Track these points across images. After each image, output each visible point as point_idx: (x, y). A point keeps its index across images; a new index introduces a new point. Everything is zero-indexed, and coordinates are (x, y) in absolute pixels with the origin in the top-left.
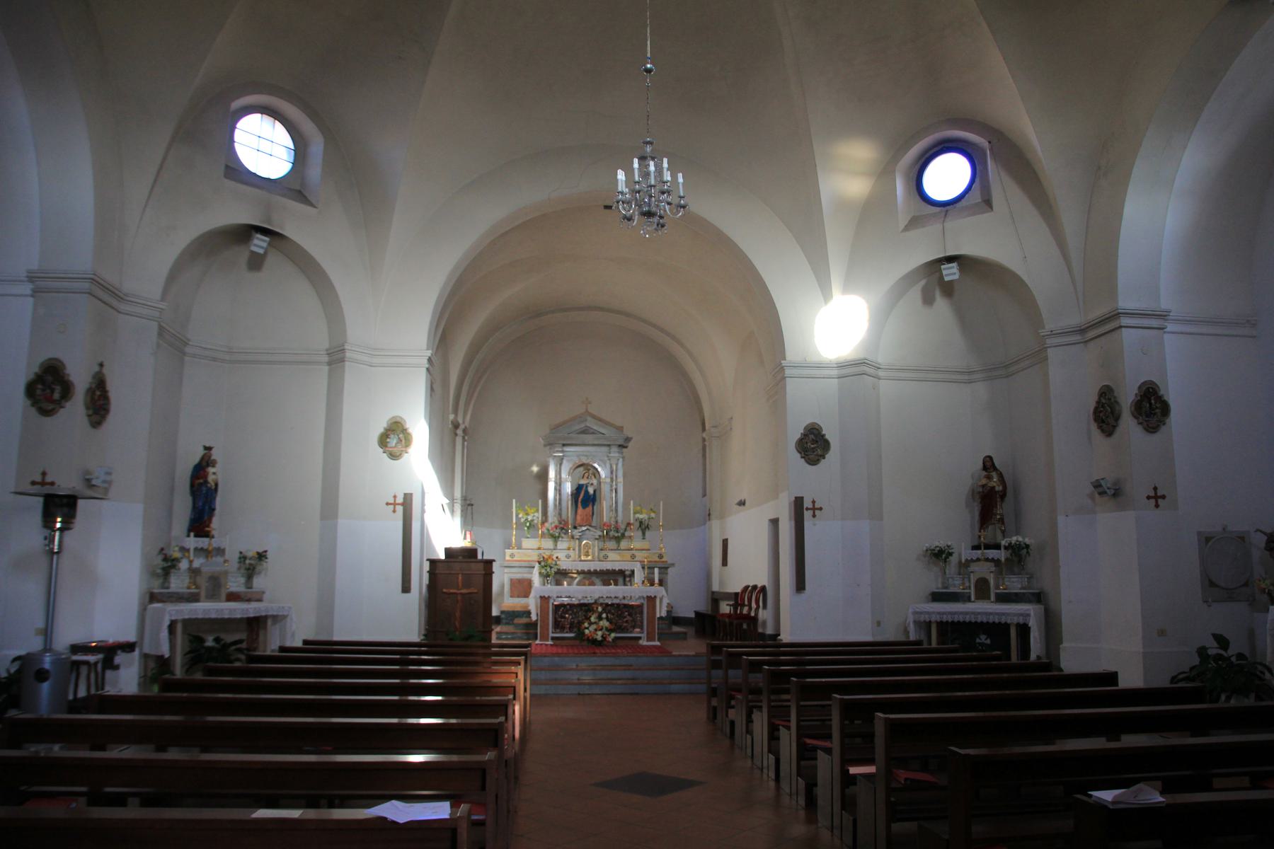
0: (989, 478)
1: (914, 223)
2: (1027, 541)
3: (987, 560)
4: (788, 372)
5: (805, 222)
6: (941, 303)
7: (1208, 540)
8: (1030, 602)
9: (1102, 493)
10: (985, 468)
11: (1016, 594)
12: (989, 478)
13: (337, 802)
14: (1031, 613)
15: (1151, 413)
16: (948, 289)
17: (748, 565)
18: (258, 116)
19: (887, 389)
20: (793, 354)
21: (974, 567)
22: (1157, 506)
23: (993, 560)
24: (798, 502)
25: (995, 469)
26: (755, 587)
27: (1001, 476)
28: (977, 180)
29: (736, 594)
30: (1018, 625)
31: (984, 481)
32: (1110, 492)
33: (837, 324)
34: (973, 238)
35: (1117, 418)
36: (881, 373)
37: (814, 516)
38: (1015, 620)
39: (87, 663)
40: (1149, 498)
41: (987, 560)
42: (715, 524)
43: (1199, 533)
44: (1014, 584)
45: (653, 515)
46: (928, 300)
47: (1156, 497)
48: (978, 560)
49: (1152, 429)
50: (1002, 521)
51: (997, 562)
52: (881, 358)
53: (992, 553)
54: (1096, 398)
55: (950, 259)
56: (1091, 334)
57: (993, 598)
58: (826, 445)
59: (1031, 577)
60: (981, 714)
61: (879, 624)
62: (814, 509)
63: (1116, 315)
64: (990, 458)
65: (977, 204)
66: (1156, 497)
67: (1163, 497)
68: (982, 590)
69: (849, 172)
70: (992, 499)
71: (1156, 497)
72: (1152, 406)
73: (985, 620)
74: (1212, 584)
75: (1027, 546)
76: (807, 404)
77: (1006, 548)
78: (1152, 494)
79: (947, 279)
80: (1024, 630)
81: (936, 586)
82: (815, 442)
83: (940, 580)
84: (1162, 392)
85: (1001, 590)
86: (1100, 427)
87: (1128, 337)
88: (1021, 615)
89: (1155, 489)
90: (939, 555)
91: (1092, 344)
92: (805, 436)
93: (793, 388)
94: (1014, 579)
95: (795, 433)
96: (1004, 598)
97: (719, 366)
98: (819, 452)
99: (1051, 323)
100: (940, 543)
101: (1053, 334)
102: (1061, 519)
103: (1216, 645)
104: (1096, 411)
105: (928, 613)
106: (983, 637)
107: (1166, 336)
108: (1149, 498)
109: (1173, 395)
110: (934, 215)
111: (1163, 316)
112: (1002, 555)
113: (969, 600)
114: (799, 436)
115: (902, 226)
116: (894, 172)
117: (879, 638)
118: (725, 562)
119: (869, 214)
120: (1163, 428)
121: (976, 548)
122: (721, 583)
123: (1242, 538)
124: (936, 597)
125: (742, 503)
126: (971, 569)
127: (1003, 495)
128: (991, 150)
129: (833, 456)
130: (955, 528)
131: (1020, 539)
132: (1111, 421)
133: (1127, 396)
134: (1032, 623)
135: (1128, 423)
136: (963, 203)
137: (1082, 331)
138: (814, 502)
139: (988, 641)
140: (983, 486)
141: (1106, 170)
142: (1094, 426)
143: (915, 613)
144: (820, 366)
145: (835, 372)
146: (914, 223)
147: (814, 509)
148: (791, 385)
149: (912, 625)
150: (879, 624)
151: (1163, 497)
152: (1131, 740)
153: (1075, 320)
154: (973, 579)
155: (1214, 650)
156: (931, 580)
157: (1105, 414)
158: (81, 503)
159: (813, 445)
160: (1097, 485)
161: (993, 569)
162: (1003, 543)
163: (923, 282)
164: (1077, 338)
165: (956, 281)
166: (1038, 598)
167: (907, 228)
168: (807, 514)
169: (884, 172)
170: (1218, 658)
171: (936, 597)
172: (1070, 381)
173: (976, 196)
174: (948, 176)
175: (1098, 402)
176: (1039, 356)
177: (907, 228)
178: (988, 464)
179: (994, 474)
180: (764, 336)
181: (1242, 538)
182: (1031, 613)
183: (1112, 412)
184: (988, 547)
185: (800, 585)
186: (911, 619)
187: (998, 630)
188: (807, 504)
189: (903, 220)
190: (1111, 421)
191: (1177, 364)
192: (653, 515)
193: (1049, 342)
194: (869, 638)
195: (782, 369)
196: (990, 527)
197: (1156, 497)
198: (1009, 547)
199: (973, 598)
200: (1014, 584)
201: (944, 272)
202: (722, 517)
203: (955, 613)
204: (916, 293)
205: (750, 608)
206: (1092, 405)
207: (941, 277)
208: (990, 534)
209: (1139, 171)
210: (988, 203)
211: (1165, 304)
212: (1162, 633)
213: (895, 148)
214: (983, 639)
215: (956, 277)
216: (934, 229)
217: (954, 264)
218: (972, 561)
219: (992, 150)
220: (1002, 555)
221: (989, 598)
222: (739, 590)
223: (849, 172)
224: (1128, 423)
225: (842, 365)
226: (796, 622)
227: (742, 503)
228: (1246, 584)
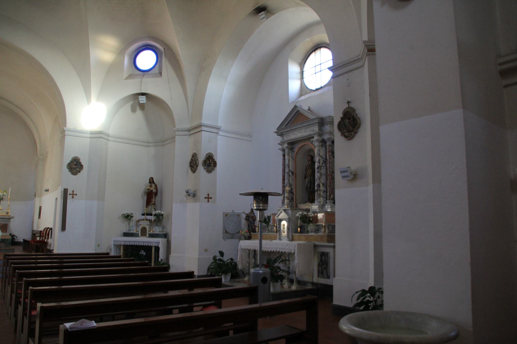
0: (151, 186)
1: (130, 76)
2: (162, 213)
3: (147, 220)
4: (66, 133)
5: (82, 67)
6: (139, 112)
7: (226, 215)
8: (162, 237)
9: (189, 195)
10: (150, 182)
11: (157, 234)
12: (151, 186)
13: (32, 327)
14: (161, 242)
15: (209, 165)
16: (142, 107)
17: (48, 219)
18: (313, 54)
19: (112, 145)
20: (70, 124)
21: (141, 223)
22: (208, 201)
23: (149, 220)
24: (65, 191)
25: (154, 183)
26: (48, 228)
27: (156, 186)
28: (158, 64)
29: (41, 231)
30: (155, 247)
31: (149, 188)
32: (192, 195)
33: (92, 113)
34: (153, 87)
35: (197, 166)
36: (110, 138)
37: (73, 197)
38: (154, 245)
39: (151, 262)
40: (205, 198)
41: (147, 220)
42: (37, 199)
43: (223, 213)
44: (157, 230)
45: (5, 193)
46: (133, 110)
47: (208, 198)
48: (143, 220)
49: (209, 171)
50: (154, 204)
51: (150, 221)
52: (110, 132)
53: (149, 217)
54: (191, 157)
55: (143, 94)
56: (192, 132)
57: (147, 235)
58: (81, 167)
59: (163, 228)
60: (141, 283)
61: (99, 245)
62: (73, 194)
63: (200, 126)
64: (152, 178)
65: (157, 73)
66: (208, 198)
67: (211, 198)
68: (144, 232)
69: (104, 49)
70: (152, 195)
71: (208, 198)
72: (210, 163)
73: (133, 244)
74: (226, 232)
75: (162, 215)
76: (74, 148)
77: (155, 215)
78: (207, 197)
79: (141, 102)
80: (157, 249)
81: (125, 230)
82: (76, 165)
83: (128, 228)
84: (214, 158)
85: (151, 232)
86: (191, 169)
87: (205, 135)
88: (157, 243)
89: (208, 195)
90: (128, 217)
91: (192, 136)
92: (72, 162)
93: (68, 140)
94: (157, 228)
95: (68, 160)
96: (152, 236)
97: (44, 127)
98: (78, 169)
99: (178, 126)
100: (129, 212)
101: (178, 130)
102: (174, 204)
103: (219, 255)
104: (191, 163)
105: (119, 241)
106: (143, 251)
107: (219, 137)
108: (205, 198)
109: (219, 159)
110: (139, 75)
111: (218, 129)
112: (152, 218)
113: (138, 236)
114: (69, 162)
115: (125, 77)
116: (124, 53)
117: (98, 251)
118: (39, 216)
119: (112, 69)
120: (213, 172)
121: (143, 215)
122: (38, 227)
123: (239, 215)
124: (126, 235)
125: (47, 190)
126: (140, 223)
127: (156, 194)
128: (164, 52)
129: (84, 172)
130: (136, 206)
131: (160, 212)
132: (195, 167)
133: (201, 158)
134: (160, 246)
135: (201, 169)
136: (151, 72)
137: (189, 130)
138: (73, 191)
139: (144, 254)
140: (148, 189)
141: (204, 69)
142: (189, 168)
143: (114, 241)
144: (82, 132)
145: (89, 136)
146: (130, 76)
147: (73, 194)
148: (67, 139)
149: (113, 246)
150: (99, 245)
151: (211, 198)
152: (172, 293)
153: (187, 126)
154: (140, 227)
155: (219, 257)
156: (124, 227)
157: (193, 165)
158: (270, 197)
159: (75, 166)
160: (187, 192)
161: (148, 224)
162: (153, 213)
163: (132, 102)
164: (187, 133)
165: (144, 102)
166: (166, 236)
167: (127, 78)
168: (69, 197)
169: (121, 53)
170: (220, 260)
171: (126, 235)
172: (182, 150)
173: (156, 70)
174: (147, 60)
175: (192, 159)
176: (173, 139)
177: (127, 78)
178: (151, 181)
179: (153, 185)
180: (59, 116)
181: (239, 215)
182: (161, 242)
183: (196, 164)
184: (148, 214)
185: (63, 228)
186: (112, 243)
187: (148, 248)
188: (70, 192)
189: (125, 75)
190: (195, 167)
191: (222, 149)
192: (5, 193)
193: (177, 133)
194: (93, 251)
195: (64, 131)
196: (150, 207)
197: (208, 198)
198: (155, 215)
199: (140, 235)
200: (157, 230)
201: (140, 99)
202: (40, 196)
203: (135, 242)
204: (128, 106)
205: (45, 238)
206: (190, 160)
207: (139, 101)
208: (151, 209)
209: (215, 71)
210: (161, 73)
211: (220, 124)
212: (206, 250)
213: (126, 43)
214: (143, 253)
215: (144, 102)
216: (137, 80)
217: (144, 97)
218: (141, 220)
219: (165, 53)
220: (152, 218)
221: (146, 235)
222: (42, 230)
223: (104, 49)
224: (201, 169)
225: (92, 133)
226: (59, 245)
227: (47, 190)
228: (238, 232)
